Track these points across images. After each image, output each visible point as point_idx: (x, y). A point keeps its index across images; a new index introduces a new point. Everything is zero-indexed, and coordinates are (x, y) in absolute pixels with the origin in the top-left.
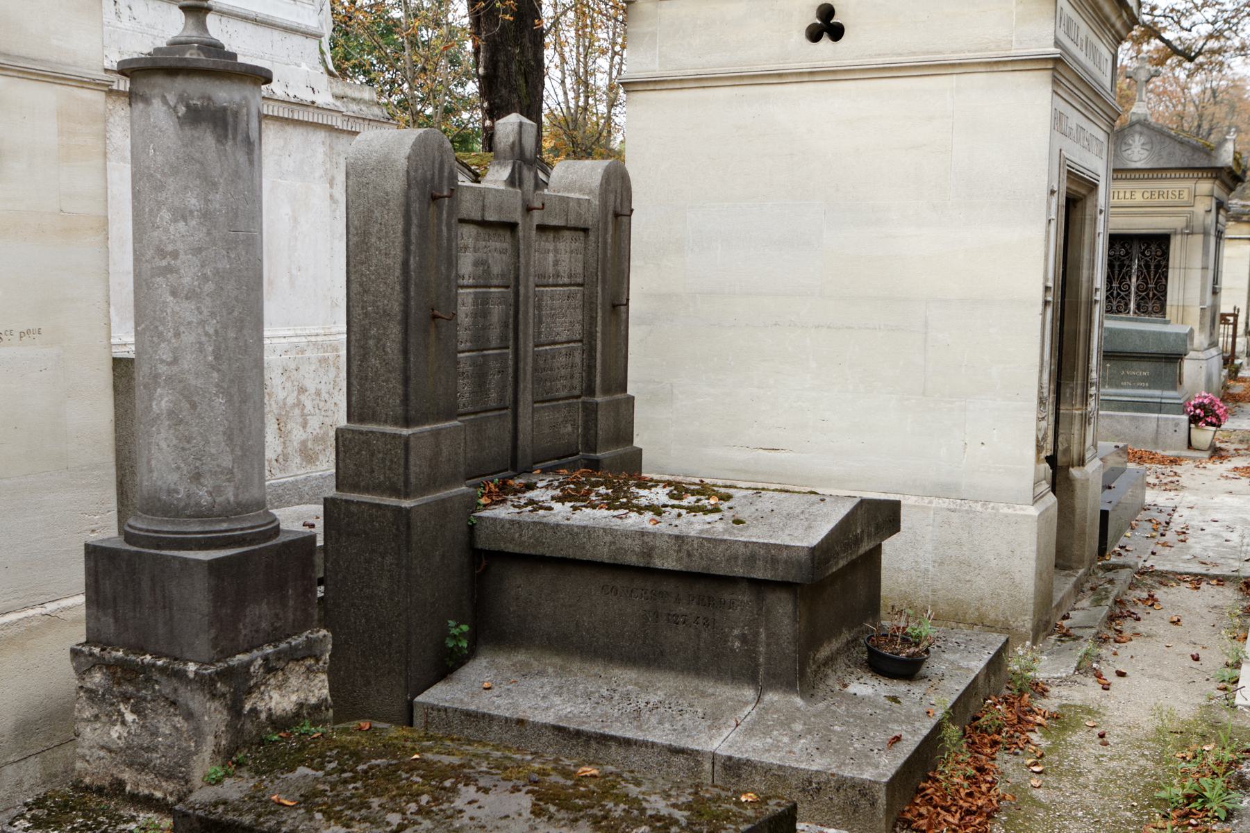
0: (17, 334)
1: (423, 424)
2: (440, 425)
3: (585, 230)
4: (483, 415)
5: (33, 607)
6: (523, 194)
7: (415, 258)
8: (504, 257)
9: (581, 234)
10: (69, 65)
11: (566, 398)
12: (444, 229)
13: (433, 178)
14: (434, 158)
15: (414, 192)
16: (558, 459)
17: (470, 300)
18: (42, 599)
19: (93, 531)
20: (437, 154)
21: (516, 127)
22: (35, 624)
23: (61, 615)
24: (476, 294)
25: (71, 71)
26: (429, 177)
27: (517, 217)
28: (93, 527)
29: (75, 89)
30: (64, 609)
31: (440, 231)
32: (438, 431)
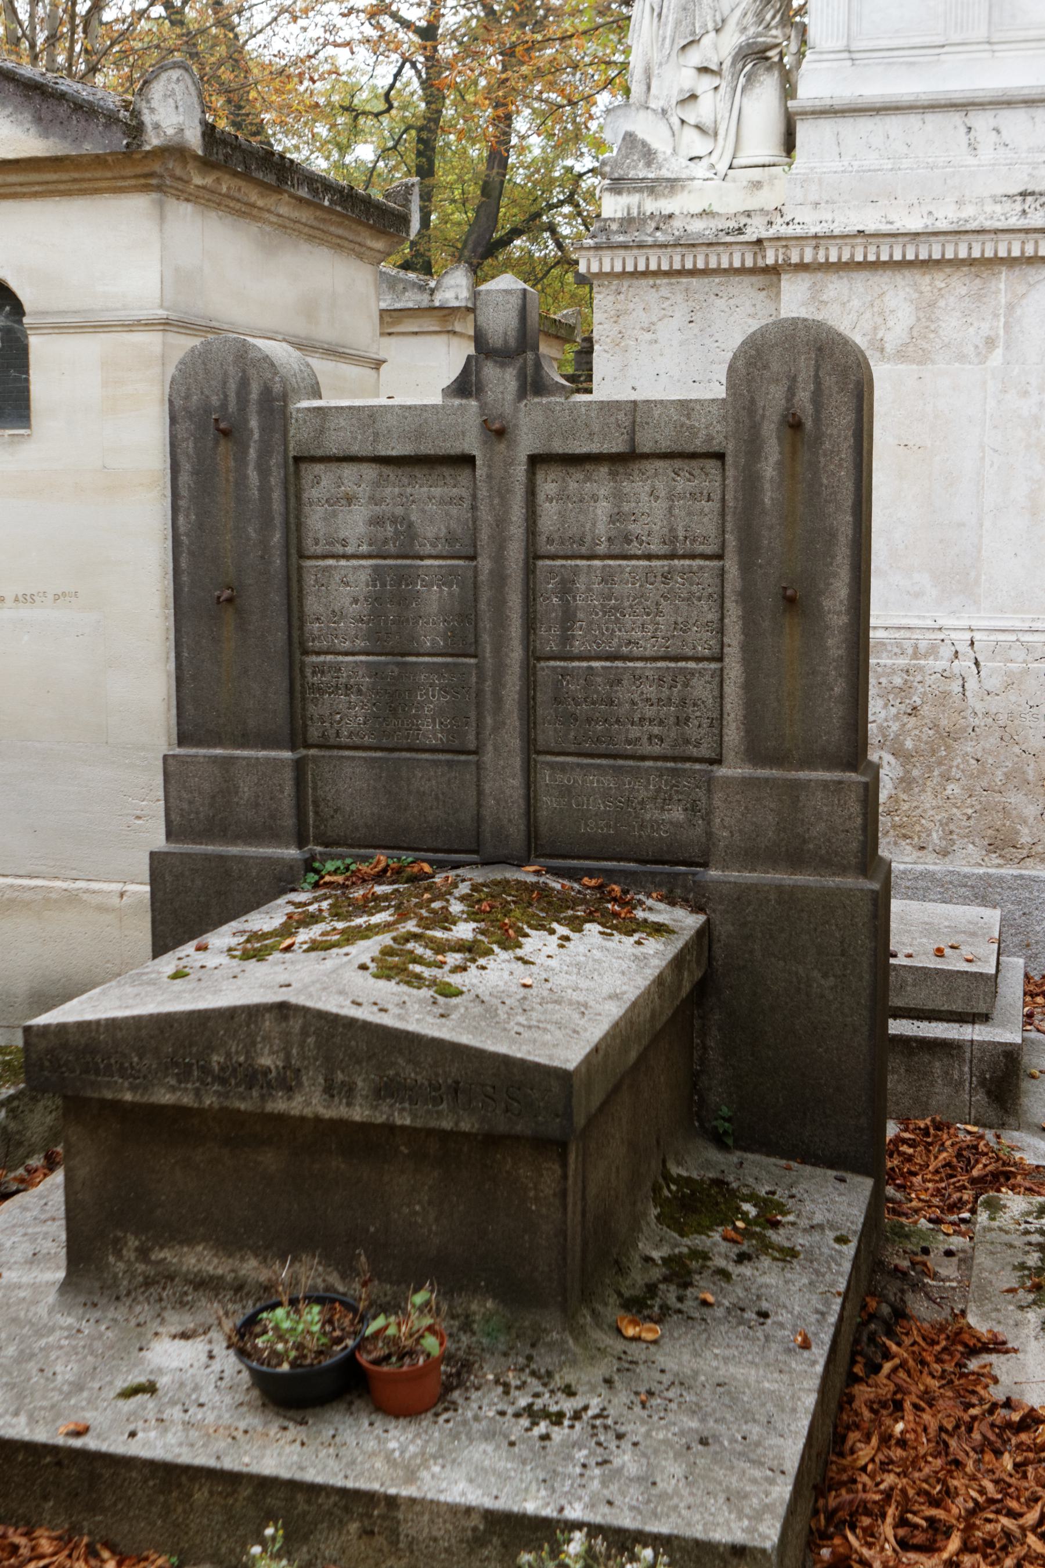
0: (51, 597)
1: (215, 746)
2: (238, 752)
3: (720, 456)
4: (408, 755)
5: (65, 880)
6: (483, 407)
7: (187, 516)
8: (454, 511)
9: (711, 465)
10: (117, 309)
11: (665, 758)
12: (253, 476)
13: (224, 405)
14: (226, 374)
15: (184, 427)
16: (637, 861)
17: (364, 577)
18: (74, 874)
19: (138, 818)
20: (232, 370)
21: (515, 301)
22: (54, 896)
23: (85, 897)
24: (376, 568)
25: (123, 315)
26: (215, 400)
27: (471, 444)
28: (138, 813)
29: (124, 334)
30: (87, 891)
31: (241, 481)
32: (231, 760)
